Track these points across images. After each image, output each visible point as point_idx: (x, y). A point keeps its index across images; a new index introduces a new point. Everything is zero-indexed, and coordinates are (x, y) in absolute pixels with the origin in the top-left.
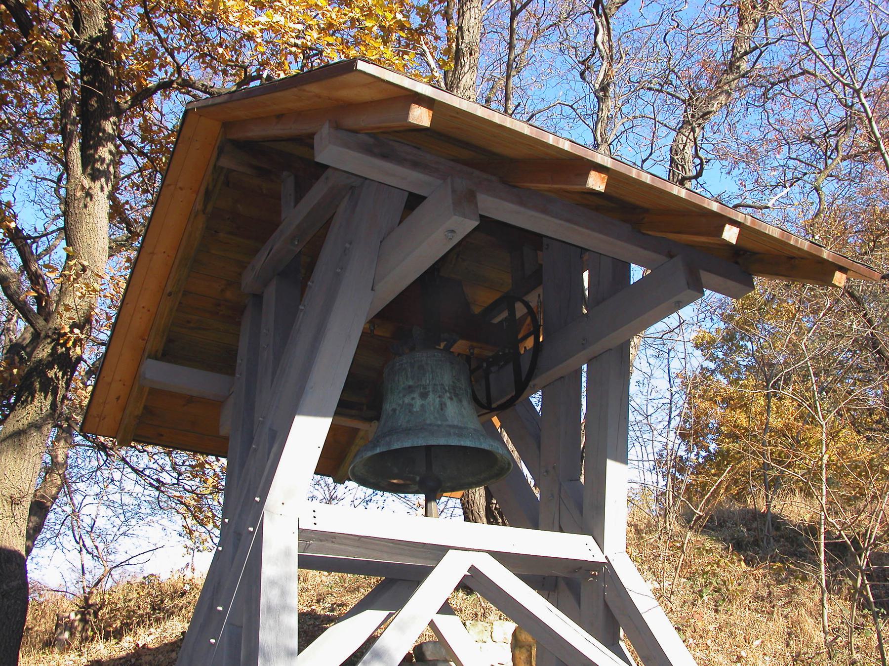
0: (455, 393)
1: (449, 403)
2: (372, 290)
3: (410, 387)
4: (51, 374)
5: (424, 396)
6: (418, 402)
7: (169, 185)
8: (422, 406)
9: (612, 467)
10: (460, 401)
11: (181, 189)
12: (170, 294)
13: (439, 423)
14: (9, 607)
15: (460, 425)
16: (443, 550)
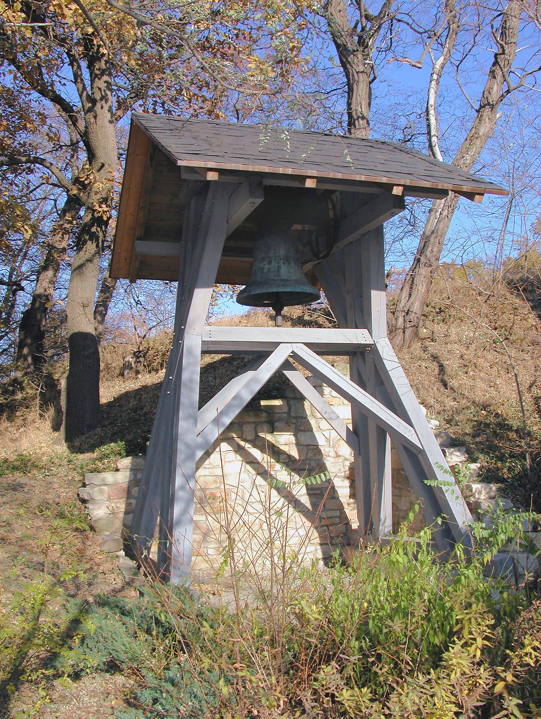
0: (287, 260)
1: (282, 266)
2: (227, 223)
3: (263, 258)
4: (94, 229)
5: (270, 263)
6: (267, 266)
7: (131, 154)
8: (268, 269)
9: (374, 294)
10: (290, 264)
11: (137, 155)
12: (142, 208)
13: (276, 278)
14: (90, 363)
15: (287, 278)
16: (278, 344)
